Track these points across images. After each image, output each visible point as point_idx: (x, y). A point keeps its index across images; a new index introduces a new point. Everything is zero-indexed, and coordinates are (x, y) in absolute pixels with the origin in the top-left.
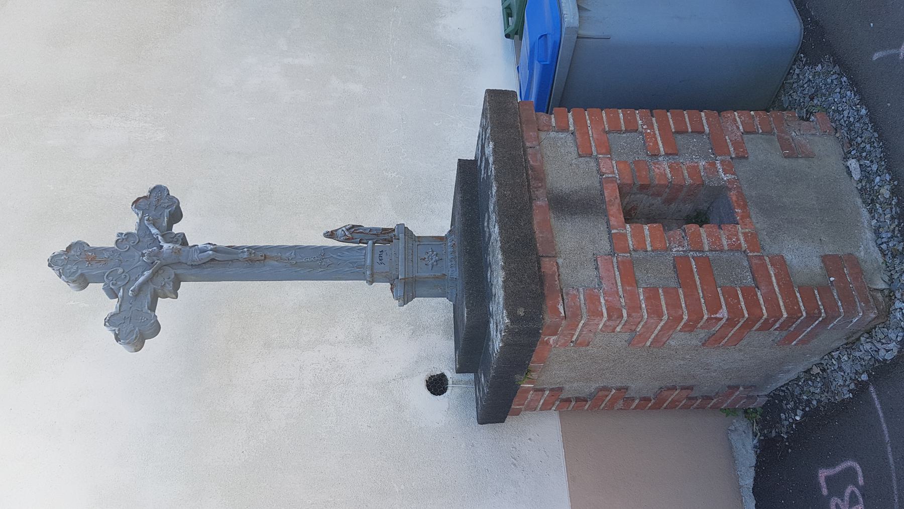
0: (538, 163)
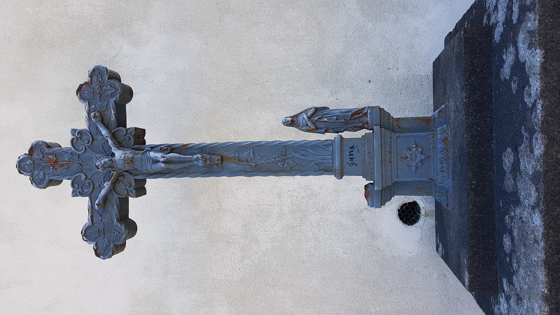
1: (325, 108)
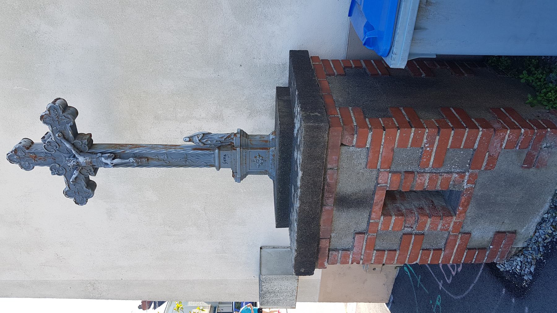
0: (333, 181)
1: (209, 133)
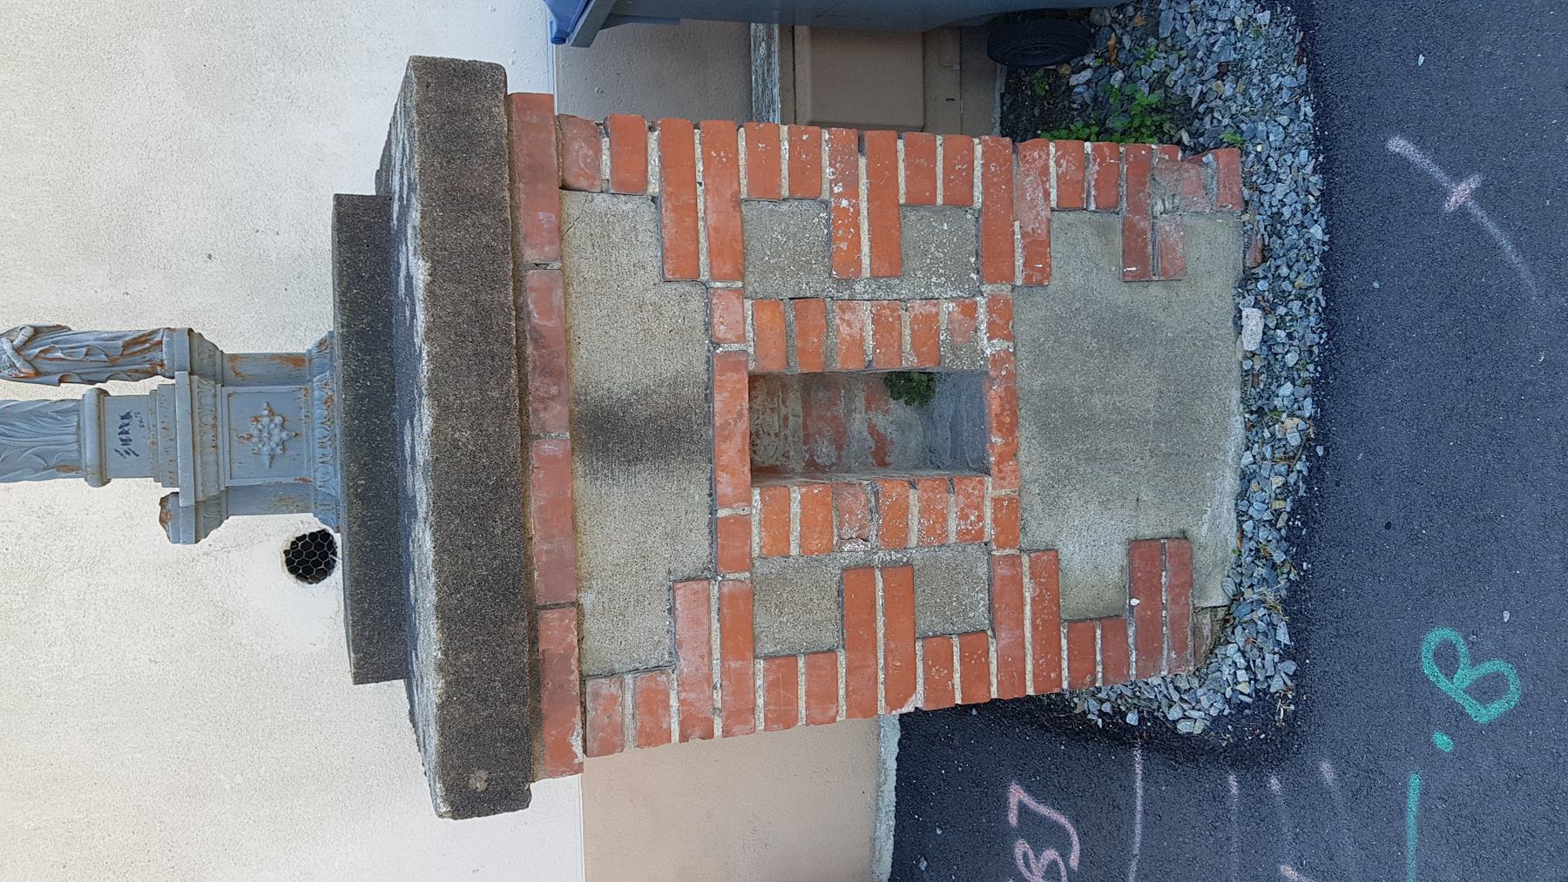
1: (59, 328)
